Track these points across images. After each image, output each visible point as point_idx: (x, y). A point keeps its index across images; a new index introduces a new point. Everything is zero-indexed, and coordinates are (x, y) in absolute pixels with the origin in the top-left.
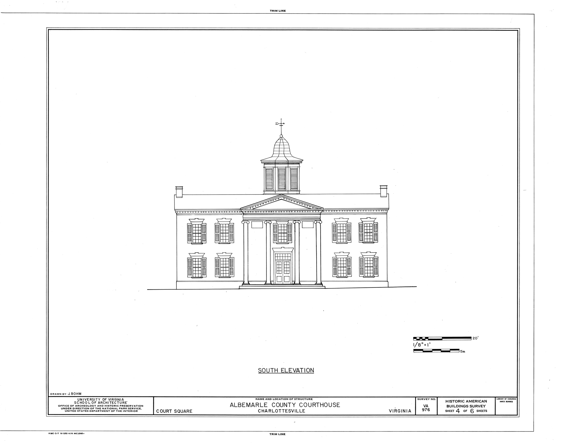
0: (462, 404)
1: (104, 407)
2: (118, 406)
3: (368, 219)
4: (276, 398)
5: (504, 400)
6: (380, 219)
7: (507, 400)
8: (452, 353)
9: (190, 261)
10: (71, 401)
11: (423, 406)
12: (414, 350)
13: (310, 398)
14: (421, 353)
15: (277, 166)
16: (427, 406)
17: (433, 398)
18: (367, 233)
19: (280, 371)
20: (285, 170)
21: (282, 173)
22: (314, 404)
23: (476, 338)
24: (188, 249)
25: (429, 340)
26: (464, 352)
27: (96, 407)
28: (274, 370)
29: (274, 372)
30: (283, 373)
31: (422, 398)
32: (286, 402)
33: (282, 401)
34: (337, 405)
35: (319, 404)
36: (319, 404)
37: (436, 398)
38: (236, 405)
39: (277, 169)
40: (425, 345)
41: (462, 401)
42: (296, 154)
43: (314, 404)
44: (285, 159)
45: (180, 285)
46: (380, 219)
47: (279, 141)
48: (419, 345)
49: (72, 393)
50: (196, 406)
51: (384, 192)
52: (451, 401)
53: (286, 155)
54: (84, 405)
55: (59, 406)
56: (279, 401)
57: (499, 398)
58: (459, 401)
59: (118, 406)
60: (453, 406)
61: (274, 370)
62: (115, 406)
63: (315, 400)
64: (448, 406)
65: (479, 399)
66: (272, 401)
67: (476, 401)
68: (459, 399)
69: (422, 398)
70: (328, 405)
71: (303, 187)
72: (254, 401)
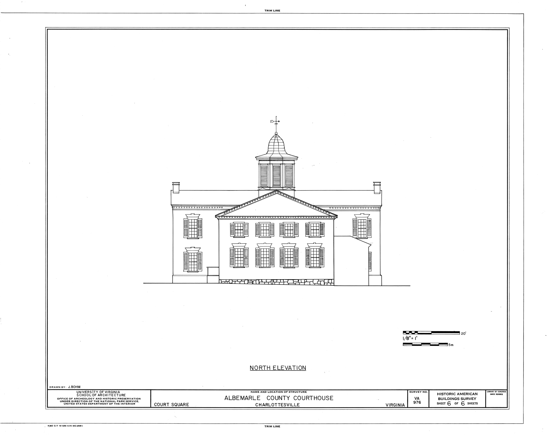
0: (453, 396)
1: (102, 400)
2: (116, 399)
3: (361, 216)
4: (271, 391)
5: (494, 393)
6: (374, 216)
7: (497, 393)
8: (441, 347)
9: (186, 255)
10: (73, 394)
11: (411, 400)
12: (404, 344)
13: (305, 391)
14: (410, 347)
15: (271, 162)
16: (418, 398)
17: (424, 391)
18: (361, 228)
19: (272, 369)
20: (280, 167)
21: (277, 174)
22: (307, 398)
23: (464, 334)
24: (183, 243)
25: (419, 334)
26: (452, 345)
27: (95, 399)
28: (266, 367)
29: (266, 369)
30: (275, 370)
31: (414, 391)
32: (281, 394)
33: (277, 394)
34: (331, 398)
35: (313, 398)
36: (313, 398)
37: (428, 391)
38: (231, 398)
39: (271, 165)
40: (412, 338)
41: (453, 394)
42: (291, 150)
43: (307, 398)
44: (279, 156)
45: (176, 280)
46: (374, 216)
47: (274, 138)
48: (408, 338)
49: (72, 387)
50: (192, 399)
51: (377, 189)
52: (442, 394)
53: (280, 152)
54: (85, 398)
55: (58, 399)
56: (274, 394)
57: (490, 390)
58: (450, 394)
59: (116, 399)
60: (445, 399)
61: (266, 367)
62: (113, 398)
63: (309, 393)
64: (439, 399)
65: (453, 392)
66: (267, 394)
67: (467, 394)
68: (450, 392)
69: (414, 391)
70: (322, 398)
71: (297, 185)
72: (248, 393)
